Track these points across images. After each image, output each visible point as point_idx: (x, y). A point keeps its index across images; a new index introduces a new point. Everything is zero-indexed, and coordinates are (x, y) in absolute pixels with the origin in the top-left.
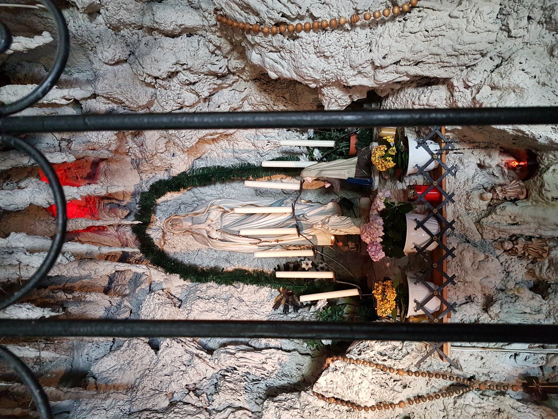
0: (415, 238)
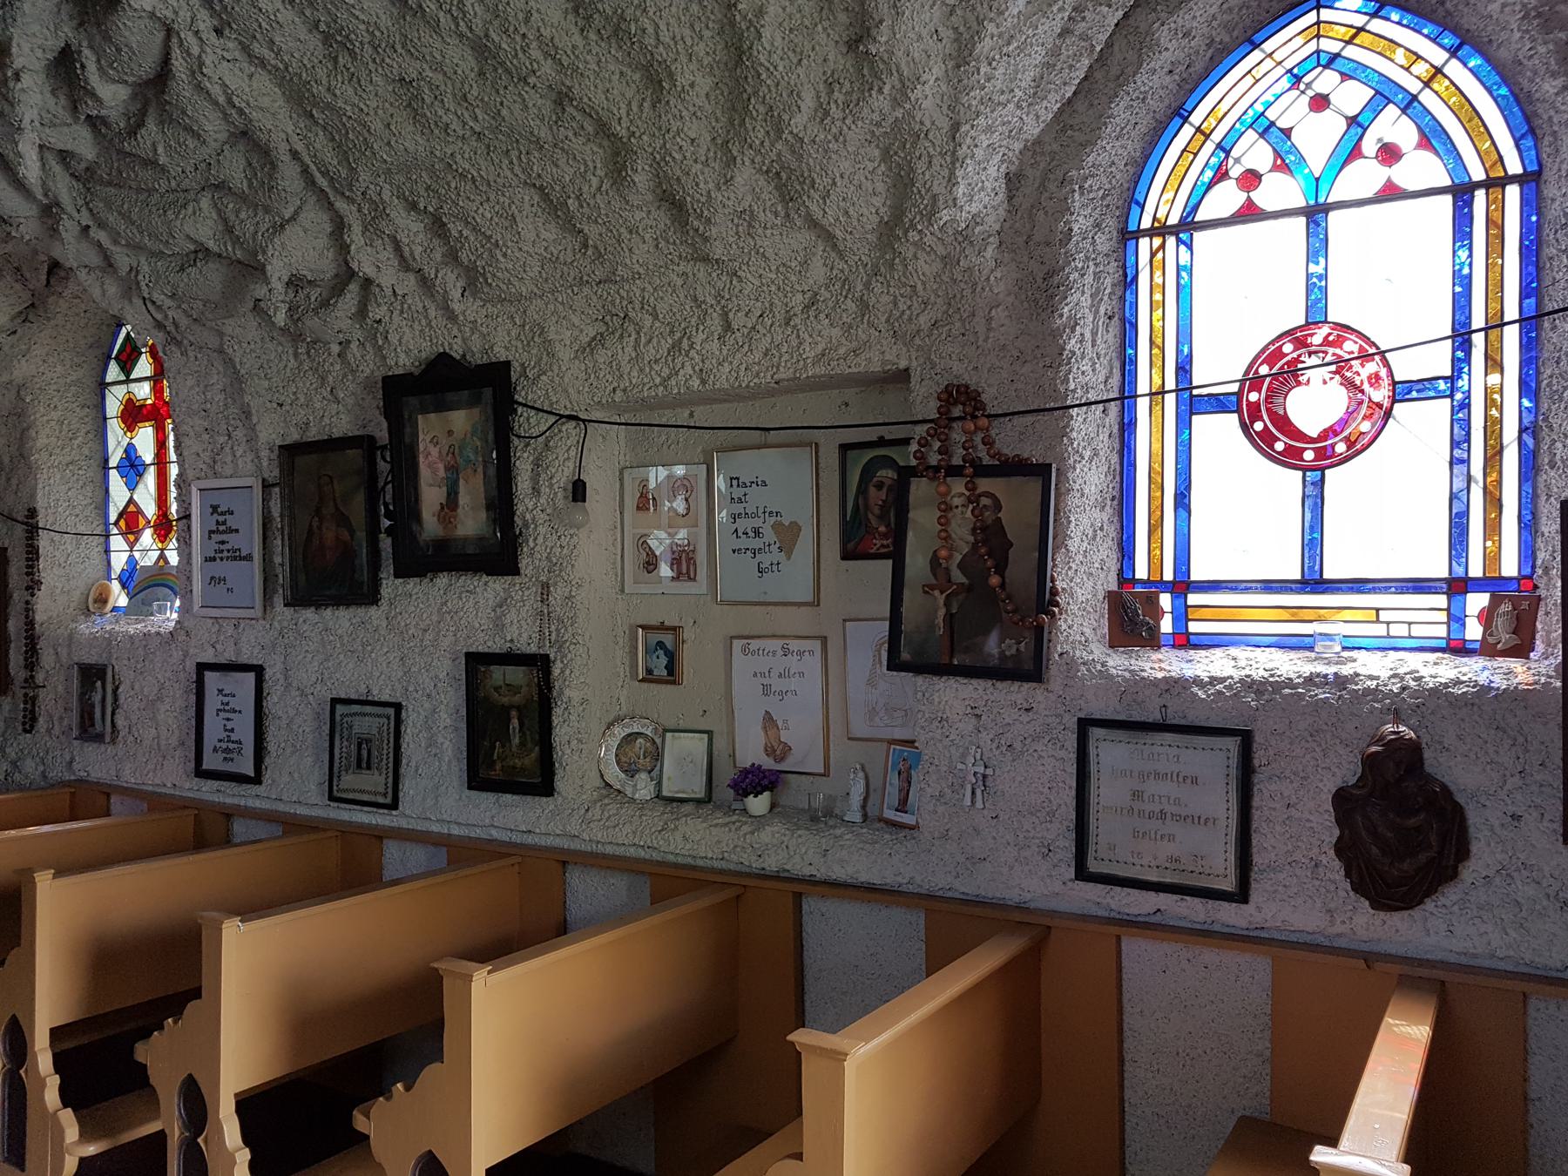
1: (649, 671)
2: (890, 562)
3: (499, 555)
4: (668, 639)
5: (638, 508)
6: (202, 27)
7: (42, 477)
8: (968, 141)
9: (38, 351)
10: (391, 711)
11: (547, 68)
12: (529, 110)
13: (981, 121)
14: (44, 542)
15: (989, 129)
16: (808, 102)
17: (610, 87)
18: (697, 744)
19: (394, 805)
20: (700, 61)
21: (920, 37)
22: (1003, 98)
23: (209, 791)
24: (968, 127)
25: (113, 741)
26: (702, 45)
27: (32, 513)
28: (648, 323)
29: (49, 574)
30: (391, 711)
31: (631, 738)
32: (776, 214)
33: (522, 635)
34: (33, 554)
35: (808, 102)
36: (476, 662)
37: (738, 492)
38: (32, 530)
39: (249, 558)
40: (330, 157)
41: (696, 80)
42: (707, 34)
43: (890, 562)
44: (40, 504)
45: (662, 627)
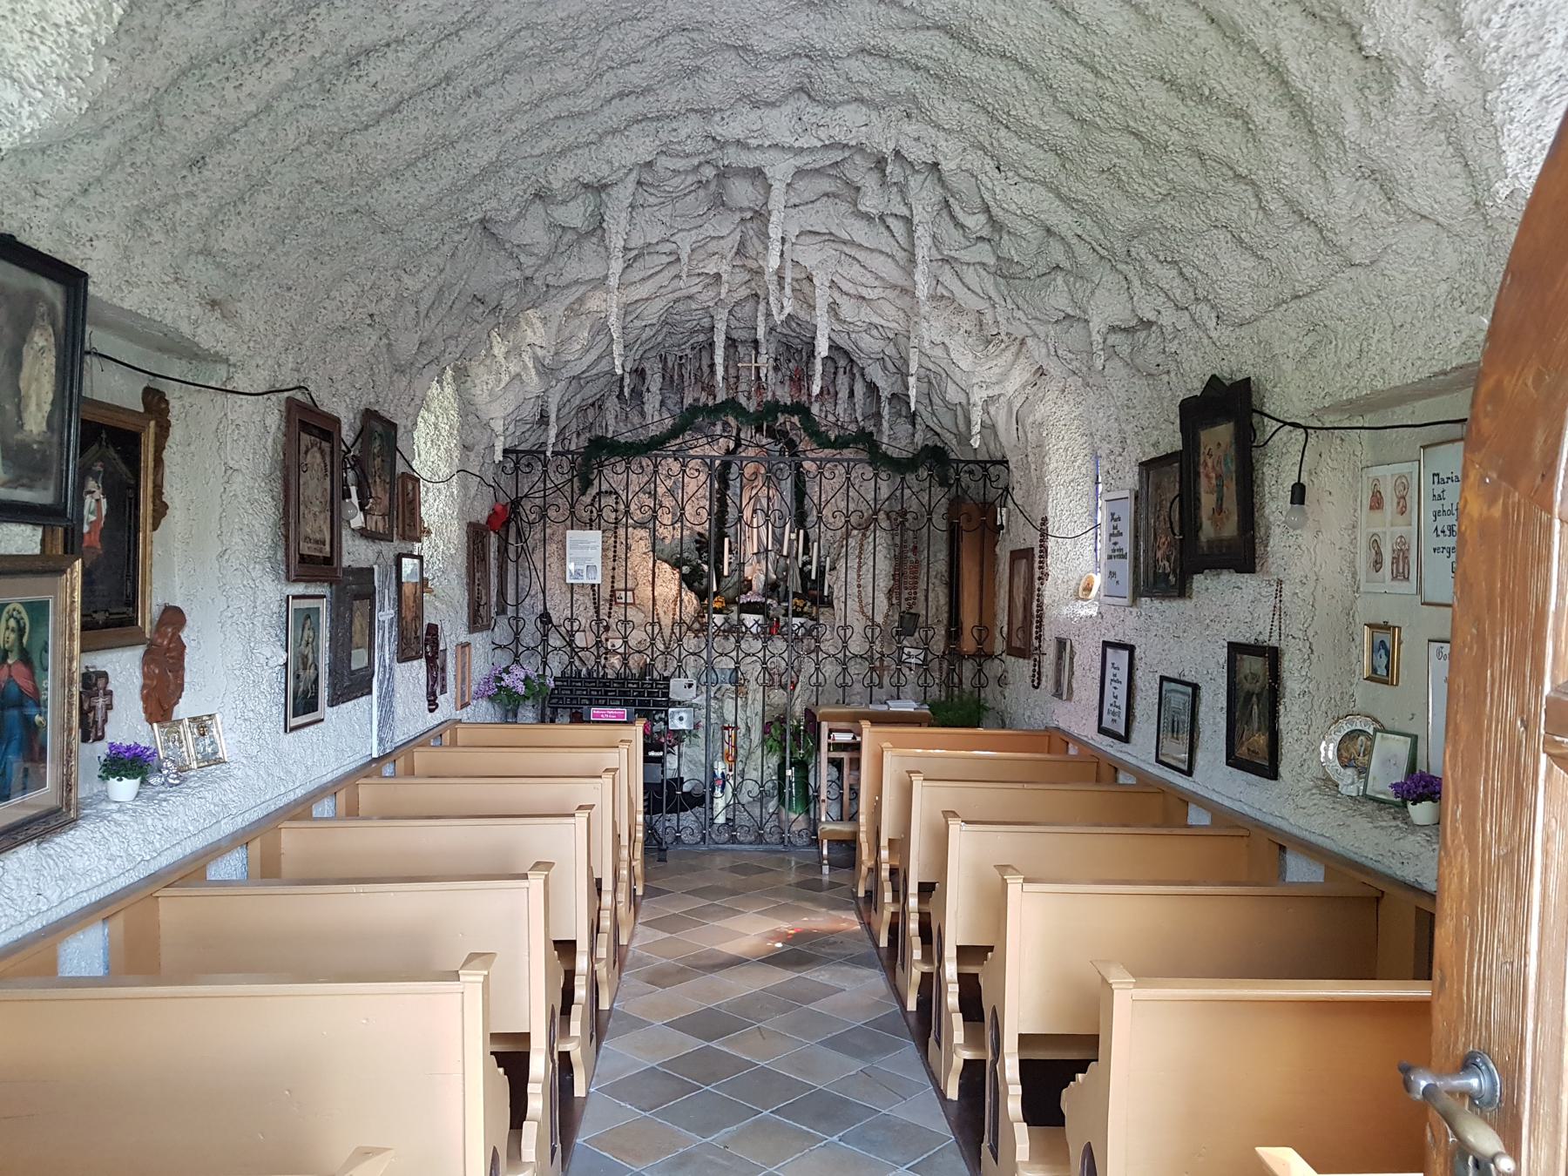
0: (750, 619)
1: (1374, 670)
2: (37, 551)
3: (1242, 555)
4: (1387, 638)
5: (1371, 508)
6: (987, 168)
7: (1052, 493)
8: (1501, 107)
9: (1050, 396)
10: (1190, 690)
11: (1175, 136)
12: (1188, 172)
13: (1512, 81)
14: (1051, 543)
15: (1530, 86)
16: (1351, 112)
17: (1223, 140)
18: (1400, 747)
19: (1189, 773)
20: (1267, 99)
21: (1405, 28)
22: (1532, 49)
23: (1104, 743)
24: (1496, 93)
25: (1069, 699)
26: (1263, 87)
27: (1045, 520)
28: (1340, 329)
29: (1054, 566)
30: (1190, 690)
31: (1353, 735)
32: (1387, 213)
33: (1258, 630)
34: (1044, 551)
35: (1351, 112)
36: (1235, 649)
37: (1438, 489)
38: (1044, 535)
39: (1124, 557)
40: (1096, 232)
41: (1272, 117)
42: (1262, 75)
43: (37, 551)
44: (1050, 514)
45: (1386, 627)
